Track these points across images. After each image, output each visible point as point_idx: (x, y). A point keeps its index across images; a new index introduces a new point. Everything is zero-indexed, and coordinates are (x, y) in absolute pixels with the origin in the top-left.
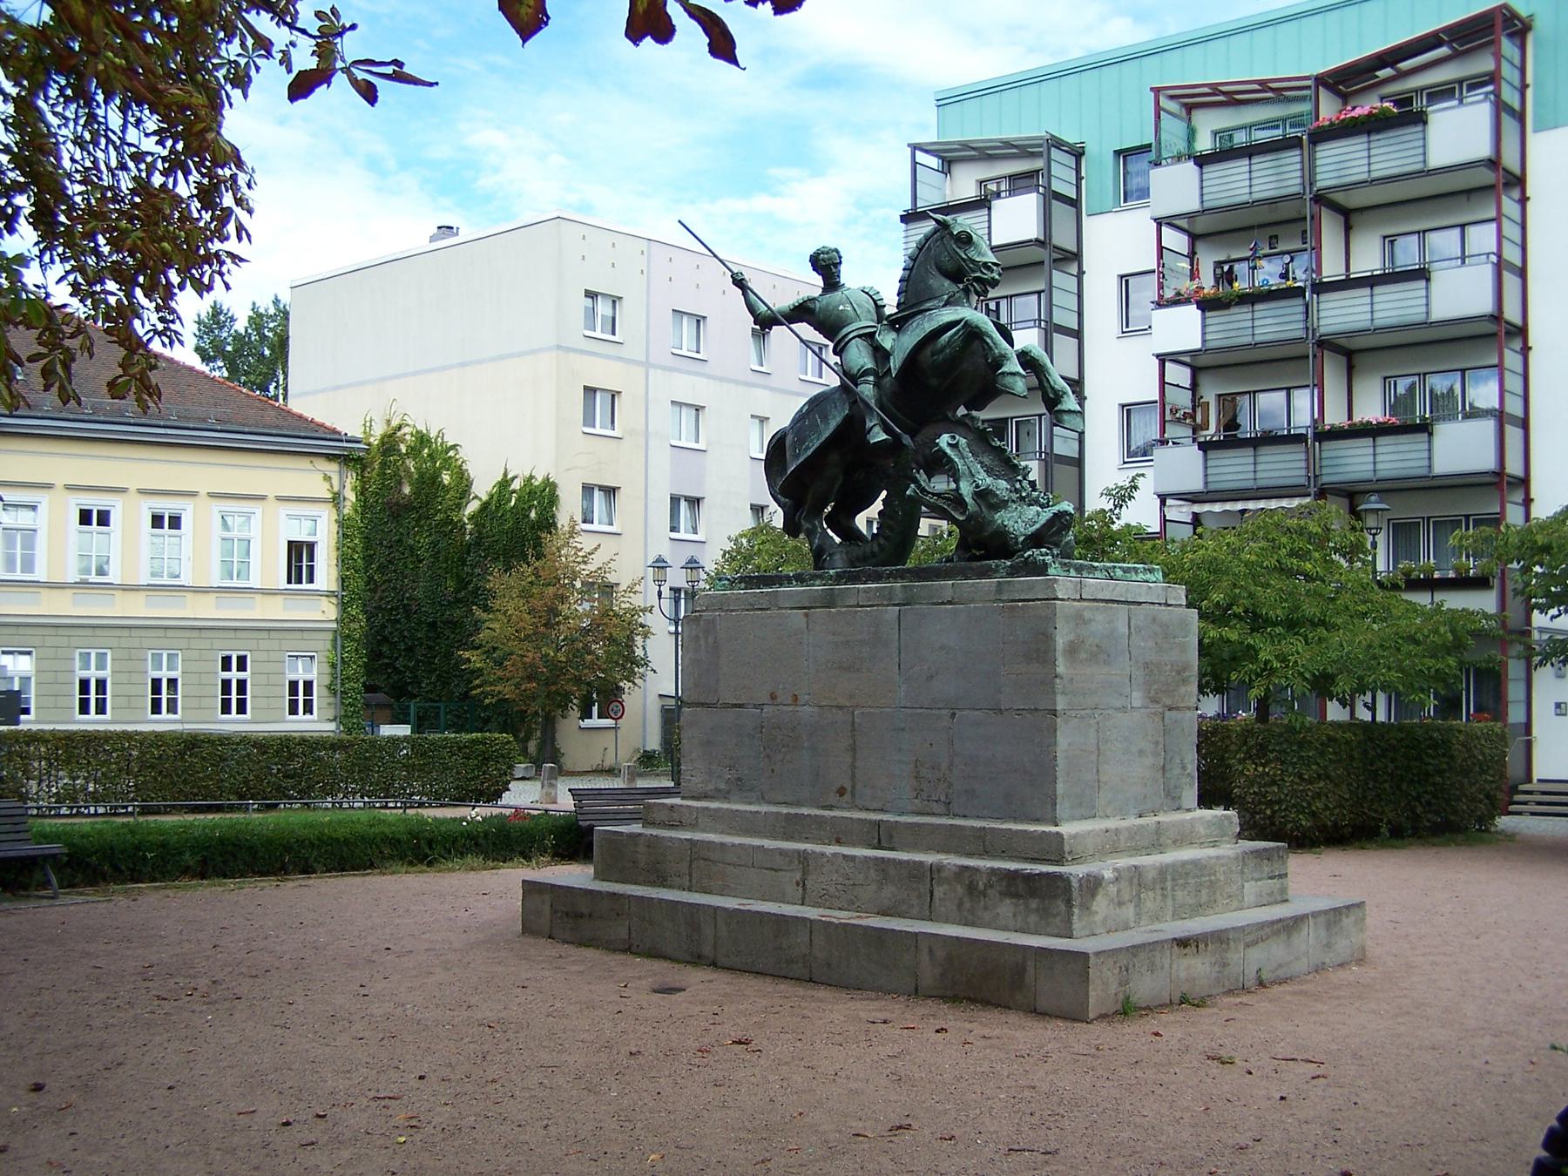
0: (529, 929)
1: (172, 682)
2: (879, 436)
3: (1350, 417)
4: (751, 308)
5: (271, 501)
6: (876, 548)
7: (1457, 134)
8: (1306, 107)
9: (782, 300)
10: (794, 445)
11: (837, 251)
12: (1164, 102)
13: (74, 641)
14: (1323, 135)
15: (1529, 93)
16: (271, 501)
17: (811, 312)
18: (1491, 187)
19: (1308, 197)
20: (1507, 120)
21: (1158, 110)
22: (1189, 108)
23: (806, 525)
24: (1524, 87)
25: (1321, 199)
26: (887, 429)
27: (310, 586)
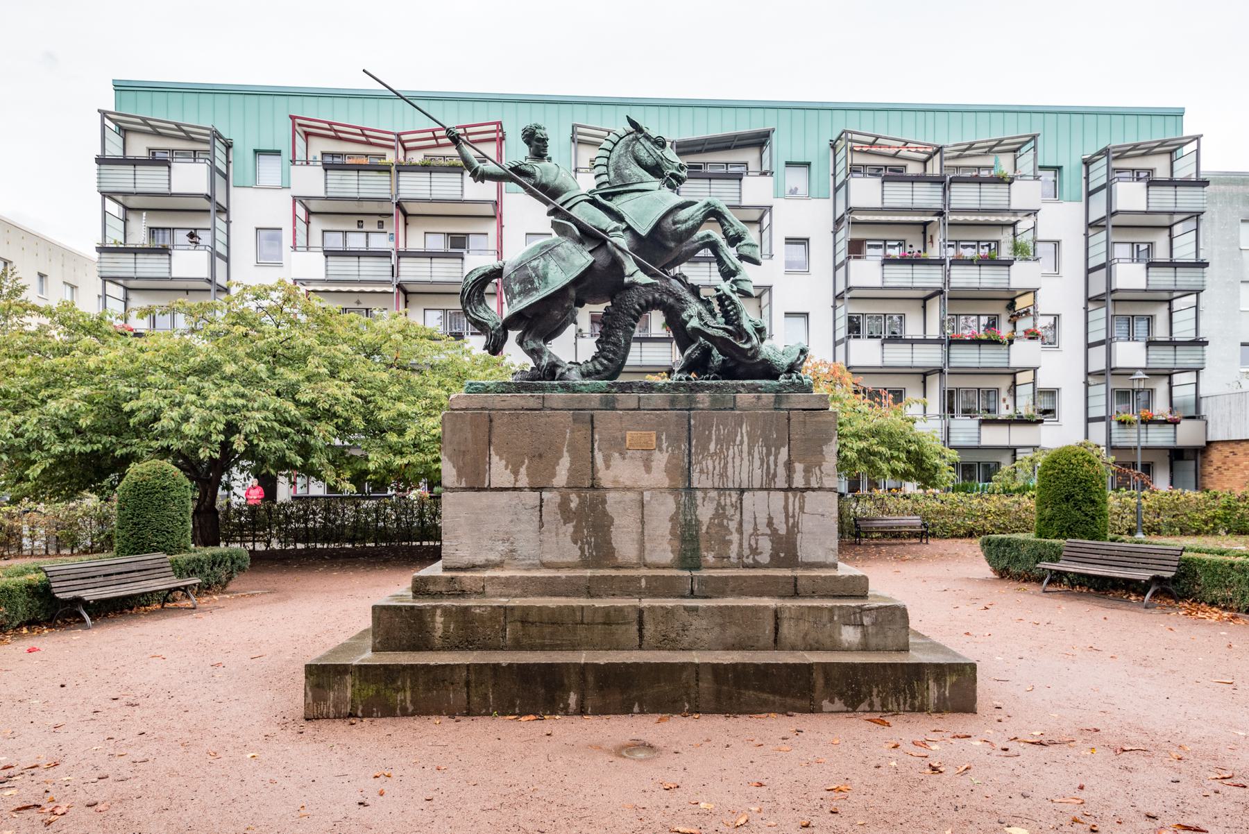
19: (394, 201)
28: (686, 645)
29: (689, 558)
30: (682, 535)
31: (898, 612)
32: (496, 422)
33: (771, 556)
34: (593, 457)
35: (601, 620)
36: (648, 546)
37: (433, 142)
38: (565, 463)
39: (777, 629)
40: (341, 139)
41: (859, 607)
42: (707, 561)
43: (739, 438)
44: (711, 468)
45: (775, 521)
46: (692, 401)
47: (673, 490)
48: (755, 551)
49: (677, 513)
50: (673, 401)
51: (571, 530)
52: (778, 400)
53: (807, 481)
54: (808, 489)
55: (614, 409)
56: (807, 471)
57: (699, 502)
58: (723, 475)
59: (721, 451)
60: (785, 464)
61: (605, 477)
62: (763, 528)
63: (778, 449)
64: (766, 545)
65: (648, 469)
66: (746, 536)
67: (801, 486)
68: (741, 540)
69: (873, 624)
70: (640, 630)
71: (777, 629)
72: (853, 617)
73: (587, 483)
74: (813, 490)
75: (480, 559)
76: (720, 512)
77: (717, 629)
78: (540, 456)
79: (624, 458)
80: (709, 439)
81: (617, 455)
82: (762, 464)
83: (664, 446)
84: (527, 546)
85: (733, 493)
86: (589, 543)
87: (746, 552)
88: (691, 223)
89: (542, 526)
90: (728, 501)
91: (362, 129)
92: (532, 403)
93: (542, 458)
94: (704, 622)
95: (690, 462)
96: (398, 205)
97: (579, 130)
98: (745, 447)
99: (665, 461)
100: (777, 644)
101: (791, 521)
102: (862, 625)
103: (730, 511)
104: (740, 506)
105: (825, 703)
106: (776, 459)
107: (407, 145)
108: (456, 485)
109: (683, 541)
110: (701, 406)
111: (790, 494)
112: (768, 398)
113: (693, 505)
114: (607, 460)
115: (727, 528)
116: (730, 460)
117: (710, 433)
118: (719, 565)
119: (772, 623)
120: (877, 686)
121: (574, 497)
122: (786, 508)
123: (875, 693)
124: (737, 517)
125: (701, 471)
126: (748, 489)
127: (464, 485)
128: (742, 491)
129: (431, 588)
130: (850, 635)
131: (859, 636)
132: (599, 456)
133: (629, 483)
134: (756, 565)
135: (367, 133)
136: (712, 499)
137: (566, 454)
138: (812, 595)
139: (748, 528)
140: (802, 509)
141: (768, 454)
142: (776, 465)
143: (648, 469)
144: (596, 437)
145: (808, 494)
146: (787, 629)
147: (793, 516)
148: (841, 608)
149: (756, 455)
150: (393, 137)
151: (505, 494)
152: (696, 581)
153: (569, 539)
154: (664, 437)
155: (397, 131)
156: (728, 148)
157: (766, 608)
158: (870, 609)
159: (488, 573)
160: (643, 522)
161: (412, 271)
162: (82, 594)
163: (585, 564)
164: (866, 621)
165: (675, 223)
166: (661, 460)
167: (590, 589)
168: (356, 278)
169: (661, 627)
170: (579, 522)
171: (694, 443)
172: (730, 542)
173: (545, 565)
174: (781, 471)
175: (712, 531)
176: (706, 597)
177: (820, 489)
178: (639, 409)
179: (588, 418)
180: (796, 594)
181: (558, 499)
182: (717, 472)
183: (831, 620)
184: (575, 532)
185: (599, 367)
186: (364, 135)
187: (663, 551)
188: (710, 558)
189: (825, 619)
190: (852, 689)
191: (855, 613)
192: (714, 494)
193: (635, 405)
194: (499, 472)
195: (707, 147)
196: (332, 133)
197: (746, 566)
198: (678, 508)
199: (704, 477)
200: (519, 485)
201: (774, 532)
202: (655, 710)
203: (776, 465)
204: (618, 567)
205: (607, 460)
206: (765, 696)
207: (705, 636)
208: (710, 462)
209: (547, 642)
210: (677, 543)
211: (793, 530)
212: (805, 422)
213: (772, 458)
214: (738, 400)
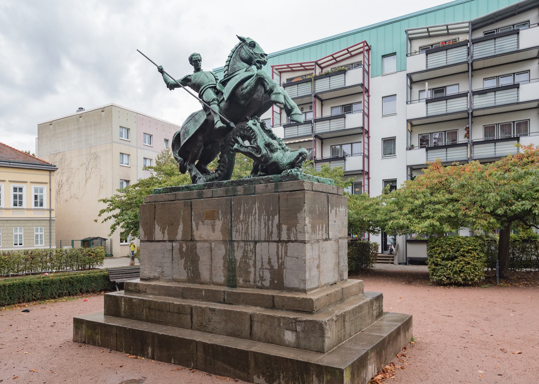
0: (75, 341)
1: (20, 236)
2: (219, 124)
3: (322, 157)
4: (166, 81)
5: (29, 183)
6: (217, 175)
7: (354, 77)
8: (313, 71)
9: (179, 77)
10: (184, 135)
11: (199, 55)
12: (274, 70)
13: (13, 225)
14: (317, 78)
15: (370, 67)
16: (29, 183)
17: (190, 80)
18: (362, 92)
19: (313, 95)
20: (366, 74)
21: (273, 72)
22: (280, 72)
23: (188, 167)
24: (369, 65)
25: (316, 96)
26: (223, 121)
27: (41, 207)
28: (210, 330)
29: (231, 282)
30: (228, 267)
31: (317, 326)
32: (157, 208)
33: (270, 282)
34: (191, 224)
35: (176, 311)
36: (214, 272)
37: (334, 61)
38: (181, 227)
39: (251, 327)
40: (294, 71)
41: (295, 319)
42: (239, 283)
43: (254, 211)
44: (241, 229)
45: (272, 261)
46: (235, 190)
47: (224, 241)
48: (262, 279)
49: (226, 255)
50: (227, 191)
51: (183, 262)
52: (276, 187)
53: (289, 236)
54: (289, 241)
55: (202, 198)
56: (289, 230)
57: (236, 248)
58: (246, 233)
59: (246, 219)
60: (277, 225)
61: (197, 235)
62: (266, 266)
63: (273, 217)
64: (267, 275)
65: (214, 231)
66: (257, 269)
67: (285, 239)
68: (255, 271)
69: (302, 331)
70: (192, 318)
71: (251, 327)
72: (292, 325)
73: (189, 239)
74: (292, 242)
75: (152, 276)
76: (245, 256)
77: (223, 323)
78: (172, 224)
79: (204, 225)
80: (240, 212)
81: (201, 223)
82: (265, 226)
83: (220, 217)
84: (168, 271)
85: (251, 244)
86: (190, 270)
87: (258, 279)
88: (249, 88)
89: (173, 260)
90: (249, 248)
91: (300, 64)
92: (172, 198)
93: (172, 226)
94: (218, 318)
95: (231, 226)
96: (316, 96)
97: (409, 32)
98: (257, 216)
99: (221, 225)
100: (251, 336)
101: (280, 261)
102: (296, 331)
103: (250, 254)
104: (254, 252)
105: (255, 377)
106: (272, 222)
107: (322, 65)
108: (144, 239)
109: (229, 271)
110: (239, 193)
111: (280, 244)
112: (271, 186)
113: (232, 250)
114: (197, 225)
115: (248, 264)
116: (250, 224)
117: (241, 208)
118: (245, 285)
119: (249, 323)
120: (283, 372)
121: (184, 245)
122: (277, 252)
123: (281, 377)
124: (253, 257)
125: (237, 231)
126: (259, 241)
127: (146, 239)
128: (256, 242)
129: (130, 288)
130: (289, 336)
131: (294, 338)
132: (194, 223)
133: (206, 238)
134: (262, 287)
135: (303, 65)
136: (241, 247)
137: (181, 223)
138: (282, 308)
139: (259, 264)
140: (286, 253)
141: (268, 220)
142: (272, 227)
143: (214, 231)
144: (193, 213)
145: (290, 245)
146: (256, 327)
147: (282, 258)
148: (284, 318)
149: (262, 221)
150: (313, 64)
151: (160, 243)
152: (226, 294)
153: (183, 267)
154: (220, 212)
155: (315, 60)
156: (513, 15)
157: (246, 313)
158: (301, 321)
159: (153, 283)
160: (211, 259)
161: (321, 128)
162: (115, 280)
163: (189, 281)
164: (299, 328)
165: (242, 90)
166: (219, 224)
167: (183, 294)
168: (296, 136)
169: (200, 318)
170: (186, 259)
171: (233, 215)
172: (250, 272)
173: (175, 280)
174: (275, 230)
175: (242, 266)
176: (231, 304)
177: (296, 241)
178: (212, 197)
179: (189, 204)
180: (273, 307)
181: (178, 247)
182: (243, 231)
183: (279, 326)
184: (185, 264)
185: (217, 175)
186: (302, 66)
187: (220, 277)
188: (241, 281)
189: (276, 324)
190: (269, 372)
191: (292, 323)
192: (242, 244)
193: (210, 195)
194: (158, 234)
195: (497, 19)
196: (289, 69)
197: (258, 287)
198: (226, 252)
199: (238, 234)
200: (165, 239)
201: (272, 267)
202: (179, 364)
203: (272, 227)
204: (202, 283)
205: (197, 225)
206: (226, 366)
207: (218, 326)
208: (240, 225)
209: (157, 319)
210: (226, 272)
211: (282, 266)
212: (287, 199)
213: (270, 222)
214: (256, 188)
